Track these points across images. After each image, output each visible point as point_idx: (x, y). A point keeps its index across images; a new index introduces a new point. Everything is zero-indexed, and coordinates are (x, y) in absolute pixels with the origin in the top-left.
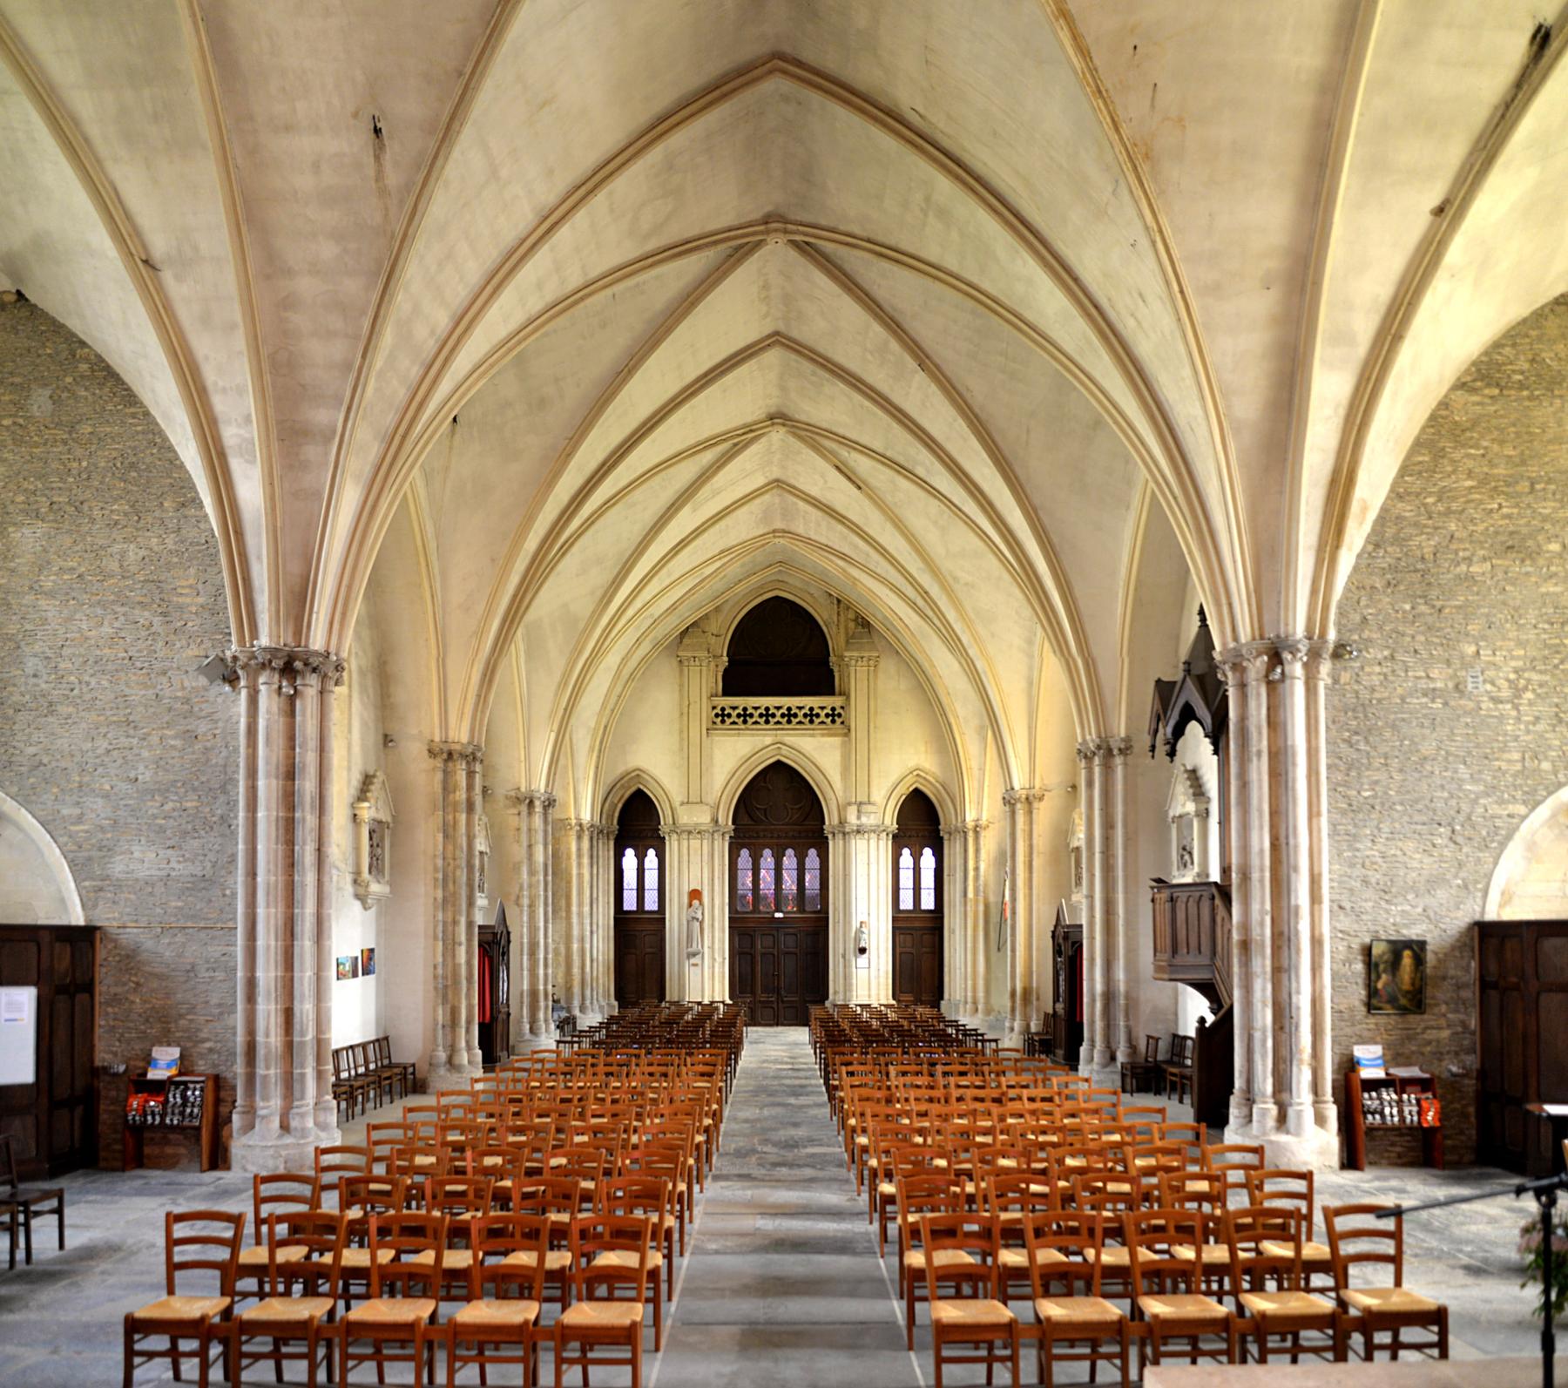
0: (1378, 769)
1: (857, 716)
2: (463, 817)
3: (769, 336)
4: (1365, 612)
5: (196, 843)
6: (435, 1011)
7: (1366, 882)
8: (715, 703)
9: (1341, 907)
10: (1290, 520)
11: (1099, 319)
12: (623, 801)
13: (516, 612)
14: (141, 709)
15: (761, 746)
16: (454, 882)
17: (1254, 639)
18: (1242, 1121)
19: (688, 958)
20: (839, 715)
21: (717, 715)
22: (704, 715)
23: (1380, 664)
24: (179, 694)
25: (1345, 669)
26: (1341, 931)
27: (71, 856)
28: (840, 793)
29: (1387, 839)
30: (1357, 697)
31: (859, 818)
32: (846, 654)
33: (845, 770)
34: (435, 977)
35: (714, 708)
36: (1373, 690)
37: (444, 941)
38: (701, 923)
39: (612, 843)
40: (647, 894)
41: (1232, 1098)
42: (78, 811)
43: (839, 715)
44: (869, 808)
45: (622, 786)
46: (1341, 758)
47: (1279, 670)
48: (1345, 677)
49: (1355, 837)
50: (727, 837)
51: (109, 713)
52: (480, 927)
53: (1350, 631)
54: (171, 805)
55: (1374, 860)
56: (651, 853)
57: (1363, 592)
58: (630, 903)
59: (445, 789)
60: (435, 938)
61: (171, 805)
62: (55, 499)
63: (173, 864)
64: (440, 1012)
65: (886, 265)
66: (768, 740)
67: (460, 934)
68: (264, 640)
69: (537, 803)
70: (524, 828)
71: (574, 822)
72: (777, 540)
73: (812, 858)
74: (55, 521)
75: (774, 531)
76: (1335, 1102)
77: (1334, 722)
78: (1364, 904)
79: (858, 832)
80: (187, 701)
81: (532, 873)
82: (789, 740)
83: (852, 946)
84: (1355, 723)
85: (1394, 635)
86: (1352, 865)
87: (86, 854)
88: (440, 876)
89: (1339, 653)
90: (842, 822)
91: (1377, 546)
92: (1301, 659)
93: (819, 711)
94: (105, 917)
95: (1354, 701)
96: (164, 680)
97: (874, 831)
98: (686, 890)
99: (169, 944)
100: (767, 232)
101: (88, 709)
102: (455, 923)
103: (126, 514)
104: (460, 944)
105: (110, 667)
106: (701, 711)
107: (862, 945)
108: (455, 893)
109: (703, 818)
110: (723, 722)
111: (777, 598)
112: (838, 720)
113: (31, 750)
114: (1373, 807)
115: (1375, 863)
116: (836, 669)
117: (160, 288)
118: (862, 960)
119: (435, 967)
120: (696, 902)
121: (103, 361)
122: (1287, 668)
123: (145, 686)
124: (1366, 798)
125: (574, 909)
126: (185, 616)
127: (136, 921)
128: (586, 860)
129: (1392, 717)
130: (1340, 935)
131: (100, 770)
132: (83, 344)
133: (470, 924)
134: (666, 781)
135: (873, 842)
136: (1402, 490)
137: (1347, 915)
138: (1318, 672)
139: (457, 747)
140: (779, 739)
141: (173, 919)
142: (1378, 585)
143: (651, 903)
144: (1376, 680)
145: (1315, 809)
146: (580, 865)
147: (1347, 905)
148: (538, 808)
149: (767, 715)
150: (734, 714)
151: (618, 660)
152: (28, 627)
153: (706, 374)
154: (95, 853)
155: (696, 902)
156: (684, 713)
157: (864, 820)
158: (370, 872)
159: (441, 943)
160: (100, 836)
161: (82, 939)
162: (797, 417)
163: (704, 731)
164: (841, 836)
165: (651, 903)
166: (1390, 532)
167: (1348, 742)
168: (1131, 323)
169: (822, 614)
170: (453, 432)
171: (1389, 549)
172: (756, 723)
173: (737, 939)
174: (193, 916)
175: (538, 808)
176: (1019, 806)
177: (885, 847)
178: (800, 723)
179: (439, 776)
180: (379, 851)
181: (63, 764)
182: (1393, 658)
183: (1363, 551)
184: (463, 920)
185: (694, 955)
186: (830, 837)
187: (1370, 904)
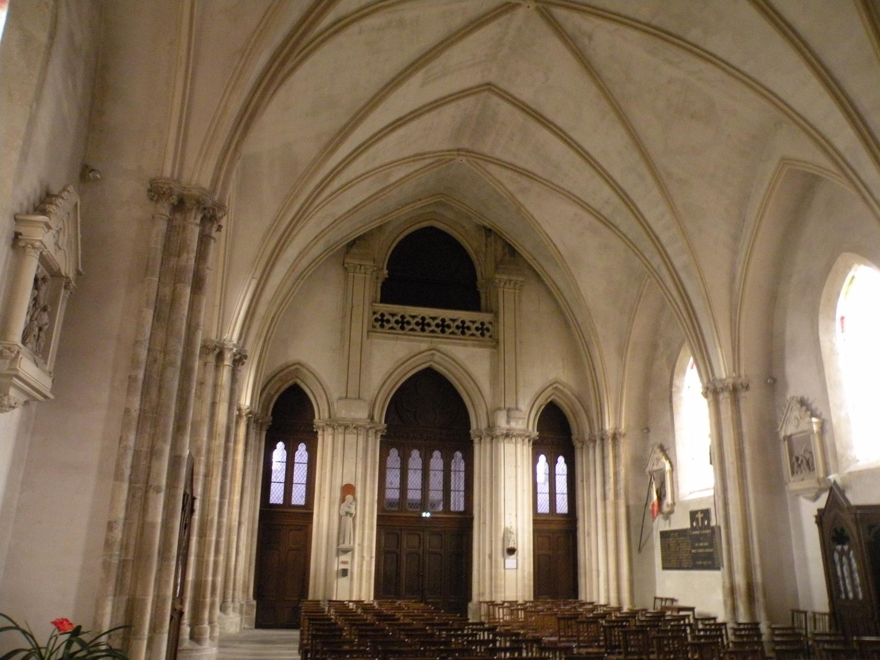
1: (506, 332)
12: (279, 394)
15: (417, 351)
16: (160, 388)
19: (338, 555)
21: (376, 320)
22: (366, 320)
31: (508, 422)
33: (495, 378)
34: (108, 544)
35: (374, 313)
38: (354, 519)
50: (379, 434)
56: (302, 447)
58: (277, 495)
59: (167, 248)
60: (118, 476)
64: (108, 609)
66: (424, 346)
67: (159, 474)
70: (210, 381)
73: (458, 463)
75: (458, 150)
81: (211, 435)
82: (444, 347)
83: (500, 547)
90: (491, 427)
93: (470, 324)
98: (338, 484)
102: (153, 453)
104: (158, 490)
108: (158, 405)
111: (431, 228)
112: (487, 334)
118: (511, 561)
119: (110, 526)
120: (349, 497)
143: (298, 497)
148: (228, 361)
151: (296, 254)
155: (349, 497)
156: (346, 314)
157: (513, 424)
158: (24, 341)
159: (125, 486)
163: (365, 334)
164: (488, 440)
165: (298, 497)
169: (471, 244)
172: (412, 330)
173: (383, 538)
175: (228, 361)
180: (45, 318)
185: (345, 551)
186: (476, 440)
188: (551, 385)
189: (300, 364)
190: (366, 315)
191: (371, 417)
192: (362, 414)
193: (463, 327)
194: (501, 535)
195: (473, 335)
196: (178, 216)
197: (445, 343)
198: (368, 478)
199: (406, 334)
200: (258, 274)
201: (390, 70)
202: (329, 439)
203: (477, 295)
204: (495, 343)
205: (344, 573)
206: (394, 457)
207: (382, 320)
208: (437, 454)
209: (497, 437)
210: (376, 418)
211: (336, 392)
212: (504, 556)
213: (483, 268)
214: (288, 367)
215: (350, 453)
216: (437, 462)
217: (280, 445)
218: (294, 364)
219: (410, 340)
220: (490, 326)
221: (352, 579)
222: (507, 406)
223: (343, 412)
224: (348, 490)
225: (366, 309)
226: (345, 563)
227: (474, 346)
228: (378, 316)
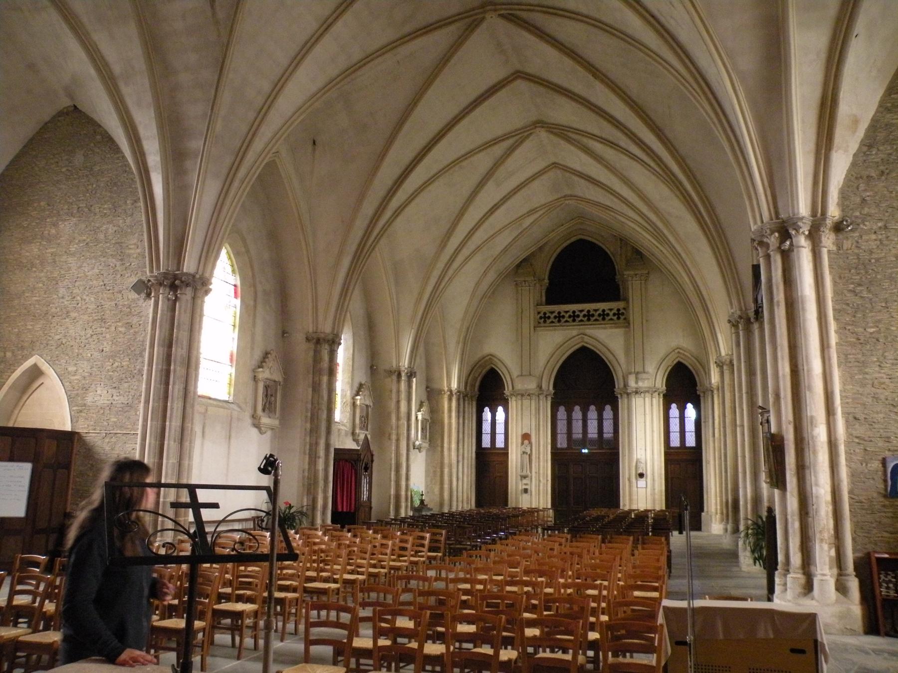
0: (880, 311)
2: (325, 379)
3: (513, 74)
4: (864, 195)
5: (126, 385)
6: (302, 499)
7: (876, 398)
8: (539, 310)
9: (855, 418)
10: (788, 135)
11: (657, 25)
13: (361, 252)
14: (108, 312)
15: (569, 337)
17: (772, 219)
18: (799, 590)
19: (521, 480)
20: (623, 314)
21: (541, 318)
22: (532, 318)
23: (875, 232)
24: (126, 303)
25: (847, 238)
26: (857, 437)
27: (69, 393)
28: (624, 366)
29: (893, 364)
30: (858, 258)
31: (637, 383)
32: (625, 273)
34: (304, 477)
35: (539, 313)
36: (871, 252)
37: (310, 455)
38: (530, 456)
39: (474, 403)
40: (497, 436)
41: (776, 573)
42: (75, 369)
43: (623, 314)
44: (644, 376)
45: (480, 366)
46: (848, 305)
47: (788, 243)
48: (847, 244)
49: (864, 364)
51: (94, 315)
52: (336, 450)
53: (852, 209)
54: (116, 364)
55: (882, 380)
57: (861, 181)
58: (486, 442)
60: (305, 453)
61: (116, 364)
62: (81, 205)
63: (115, 397)
64: (305, 500)
65: (558, 20)
66: (575, 333)
68: (161, 271)
69: (403, 374)
71: (446, 389)
72: (567, 202)
73: (608, 412)
74: (80, 217)
75: (565, 196)
76: (856, 576)
77: (840, 278)
78: (876, 415)
79: (636, 393)
80: (129, 307)
82: (588, 332)
84: (858, 277)
85: (890, 210)
86: (863, 385)
87: (75, 392)
88: (309, 414)
89: (838, 228)
90: (626, 385)
91: (870, 147)
92: (803, 233)
93: (609, 312)
94: (81, 428)
95: (857, 261)
96: (120, 296)
97: (648, 392)
98: (520, 434)
99: (109, 442)
100: (485, 12)
101: (84, 314)
102: (317, 444)
103: (110, 209)
105: (96, 290)
106: (530, 315)
107: (640, 471)
109: (531, 385)
110: (545, 322)
111: (581, 240)
112: (622, 317)
113: (58, 337)
114: (878, 340)
115: (884, 383)
116: (620, 283)
117: (118, 91)
118: (642, 483)
121: (108, 133)
122: (794, 240)
123: (110, 299)
124: (871, 333)
125: (446, 445)
126: (131, 260)
127: (95, 429)
128: (454, 414)
129: (890, 271)
130: (857, 440)
131: (87, 346)
132: (100, 126)
133: (328, 446)
134: (508, 362)
135: (648, 400)
136: (889, 105)
137: (861, 425)
138: (821, 242)
139: (322, 335)
140: (581, 331)
141: (111, 428)
142: (873, 175)
144: (873, 245)
145: (825, 343)
146: (450, 417)
147: (861, 417)
148: (404, 378)
149: (574, 316)
150: (552, 316)
152: (63, 272)
153: (475, 101)
154: (80, 392)
155: (526, 442)
157: (640, 384)
158: (264, 410)
159: (307, 457)
160: (83, 382)
161: (67, 439)
162: (549, 121)
164: (626, 395)
165: (500, 443)
166: (881, 136)
167: (853, 291)
168: (672, 22)
169: (610, 248)
170: (314, 150)
171: (881, 148)
172: (567, 321)
174: (121, 427)
176: (725, 367)
177: (657, 403)
178: (596, 320)
179: (311, 353)
181: (71, 344)
182: (886, 227)
183: (859, 150)
184: (322, 442)
185: (525, 477)
186: (619, 396)
187: (881, 416)
188: (674, 351)
189: (491, 355)
190: (532, 315)
191: (540, 387)
192: (532, 385)
193: (604, 315)
194: (634, 464)
195: (611, 319)
196: (319, 346)
197: (589, 328)
198: (541, 428)
199: (561, 326)
200: (416, 326)
201: (466, 192)
202: (514, 403)
203: (617, 288)
204: (627, 324)
205: (526, 491)
206: (562, 413)
207: (545, 317)
208: (592, 408)
209: (630, 393)
210: (544, 386)
211: (515, 373)
212: (636, 479)
213: (619, 263)
214: (484, 358)
215: (526, 413)
216: (593, 414)
217: (487, 409)
218: (488, 355)
219: (565, 330)
220: (624, 311)
221: (531, 495)
222: (636, 370)
223: (519, 386)
224: (526, 437)
225: (532, 312)
226: (526, 484)
227: (611, 328)
228: (542, 315)
